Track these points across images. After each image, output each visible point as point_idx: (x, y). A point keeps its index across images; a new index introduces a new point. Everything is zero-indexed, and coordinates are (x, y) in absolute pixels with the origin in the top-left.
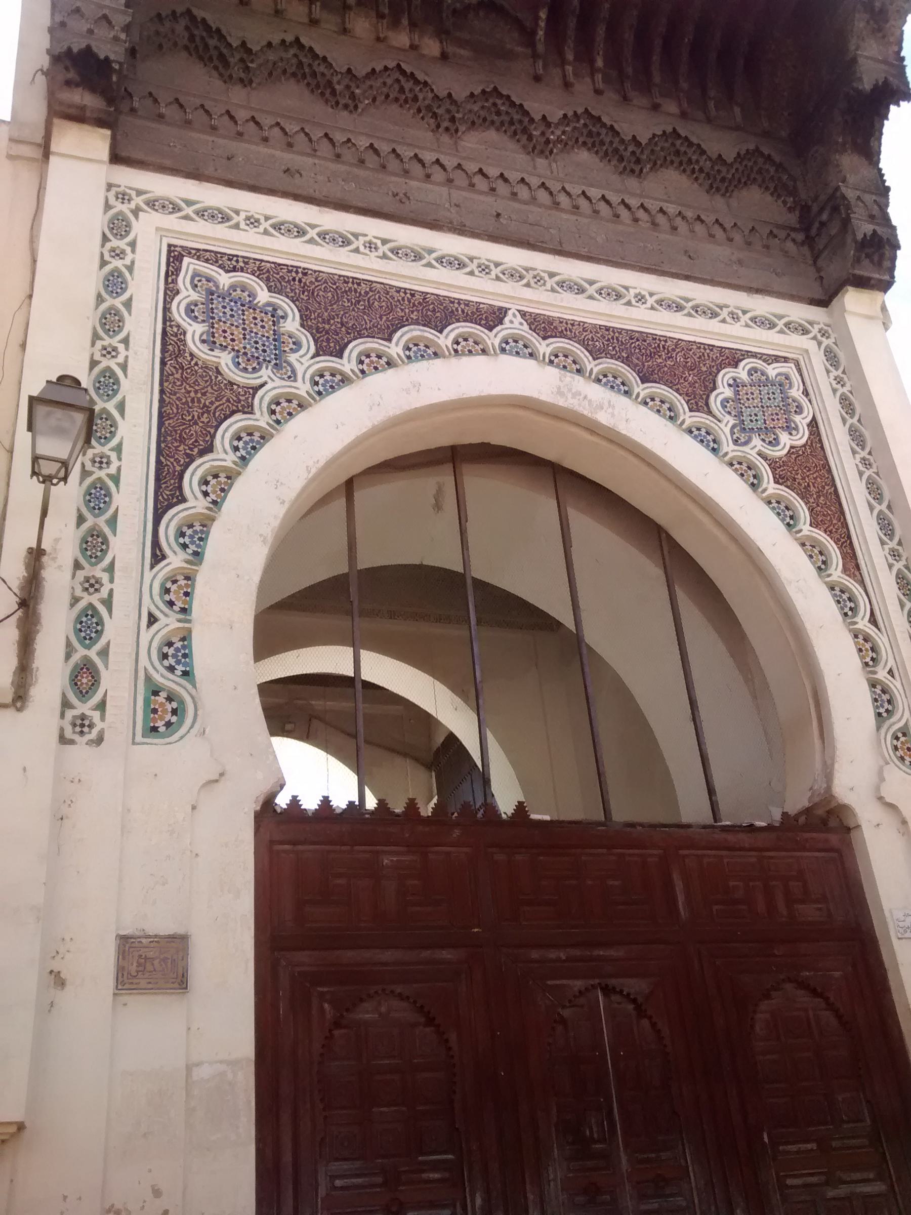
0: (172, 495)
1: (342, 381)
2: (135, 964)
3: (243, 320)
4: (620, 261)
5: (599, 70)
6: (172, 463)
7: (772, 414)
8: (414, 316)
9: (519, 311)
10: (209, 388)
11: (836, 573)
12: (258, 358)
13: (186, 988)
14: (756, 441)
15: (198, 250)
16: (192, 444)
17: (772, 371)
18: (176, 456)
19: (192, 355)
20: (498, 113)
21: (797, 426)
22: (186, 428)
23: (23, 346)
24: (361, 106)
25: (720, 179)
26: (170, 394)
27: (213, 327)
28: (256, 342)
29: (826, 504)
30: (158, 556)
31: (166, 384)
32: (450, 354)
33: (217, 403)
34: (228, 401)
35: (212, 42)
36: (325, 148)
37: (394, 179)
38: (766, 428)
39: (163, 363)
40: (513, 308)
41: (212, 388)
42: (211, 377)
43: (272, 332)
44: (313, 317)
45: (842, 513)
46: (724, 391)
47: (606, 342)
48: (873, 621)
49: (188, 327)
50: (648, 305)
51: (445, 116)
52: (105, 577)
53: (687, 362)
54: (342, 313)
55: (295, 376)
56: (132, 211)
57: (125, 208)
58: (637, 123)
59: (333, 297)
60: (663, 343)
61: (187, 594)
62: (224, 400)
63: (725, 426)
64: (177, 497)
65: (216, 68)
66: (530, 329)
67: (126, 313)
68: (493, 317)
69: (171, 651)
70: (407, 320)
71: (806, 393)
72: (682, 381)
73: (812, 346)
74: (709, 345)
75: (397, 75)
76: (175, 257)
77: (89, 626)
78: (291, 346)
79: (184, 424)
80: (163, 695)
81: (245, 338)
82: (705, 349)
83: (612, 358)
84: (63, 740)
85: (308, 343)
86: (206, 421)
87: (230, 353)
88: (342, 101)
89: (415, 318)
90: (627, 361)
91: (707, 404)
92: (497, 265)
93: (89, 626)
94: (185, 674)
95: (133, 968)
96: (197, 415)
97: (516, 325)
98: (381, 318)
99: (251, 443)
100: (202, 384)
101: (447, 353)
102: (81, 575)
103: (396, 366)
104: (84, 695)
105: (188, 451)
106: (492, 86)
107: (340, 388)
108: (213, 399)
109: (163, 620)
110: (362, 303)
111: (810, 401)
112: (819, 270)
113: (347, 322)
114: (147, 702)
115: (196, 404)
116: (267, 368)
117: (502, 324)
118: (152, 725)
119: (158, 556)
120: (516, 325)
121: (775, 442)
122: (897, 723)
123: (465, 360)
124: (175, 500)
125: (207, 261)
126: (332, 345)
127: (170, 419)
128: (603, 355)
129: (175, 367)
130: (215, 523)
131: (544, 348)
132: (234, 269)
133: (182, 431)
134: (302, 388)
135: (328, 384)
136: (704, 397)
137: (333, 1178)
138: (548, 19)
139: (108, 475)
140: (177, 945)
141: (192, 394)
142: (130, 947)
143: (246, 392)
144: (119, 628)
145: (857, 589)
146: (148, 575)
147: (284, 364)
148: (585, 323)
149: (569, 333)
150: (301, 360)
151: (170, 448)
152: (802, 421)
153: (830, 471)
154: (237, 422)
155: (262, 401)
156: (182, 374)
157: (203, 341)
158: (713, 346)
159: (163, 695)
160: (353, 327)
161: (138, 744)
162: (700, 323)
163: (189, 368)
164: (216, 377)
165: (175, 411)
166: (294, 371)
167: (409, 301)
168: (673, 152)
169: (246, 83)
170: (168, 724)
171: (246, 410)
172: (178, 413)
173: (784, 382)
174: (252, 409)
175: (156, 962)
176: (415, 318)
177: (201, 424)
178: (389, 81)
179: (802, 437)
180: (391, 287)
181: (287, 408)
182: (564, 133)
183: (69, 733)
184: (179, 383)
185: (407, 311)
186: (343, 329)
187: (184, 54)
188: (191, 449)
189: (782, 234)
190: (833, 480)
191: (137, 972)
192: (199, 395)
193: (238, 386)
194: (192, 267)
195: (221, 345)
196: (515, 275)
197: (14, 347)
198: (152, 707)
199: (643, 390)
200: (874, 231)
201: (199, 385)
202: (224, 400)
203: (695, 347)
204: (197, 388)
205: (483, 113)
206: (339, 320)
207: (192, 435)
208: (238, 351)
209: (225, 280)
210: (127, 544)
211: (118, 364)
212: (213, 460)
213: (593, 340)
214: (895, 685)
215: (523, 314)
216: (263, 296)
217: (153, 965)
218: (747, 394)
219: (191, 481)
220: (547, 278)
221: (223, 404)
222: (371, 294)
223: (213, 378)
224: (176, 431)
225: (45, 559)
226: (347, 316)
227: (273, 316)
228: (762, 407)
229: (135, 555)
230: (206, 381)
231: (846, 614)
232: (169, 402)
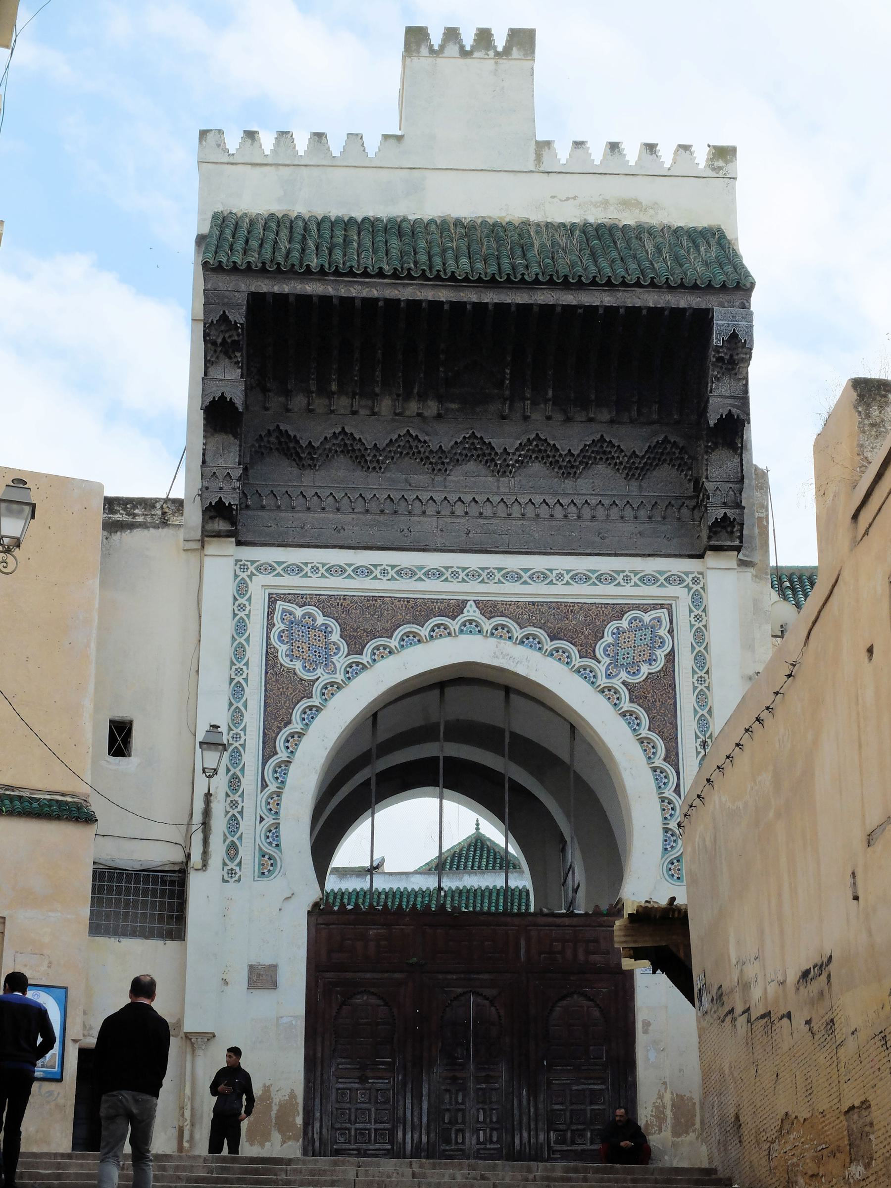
1: (362, 669)
4: (549, 551)
5: (549, 400)
11: (659, 762)
15: (285, 594)
17: (647, 618)
19: (281, 665)
20: (476, 449)
23: (198, 671)
24: (383, 466)
25: (635, 469)
30: (264, 785)
35: (291, 445)
36: (359, 506)
37: (402, 518)
39: (266, 673)
51: (439, 462)
52: (240, 800)
56: (248, 576)
57: (244, 575)
58: (572, 438)
61: (278, 804)
65: (294, 460)
67: (247, 646)
69: (270, 835)
75: (408, 438)
76: (272, 600)
77: (234, 824)
78: (335, 651)
80: (267, 857)
84: (224, 881)
85: (344, 648)
88: (371, 466)
92: (464, 569)
93: (234, 824)
94: (277, 845)
95: (255, 979)
96: (286, 699)
99: (314, 711)
102: (229, 799)
104: (232, 859)
106: (471, 432)
107: (361, 673)
109: (267, 819)
114: (260, 861)
119: (264, 785)
120: (471, 613)
123: (437, 641)
125: (289, 602)
132: (305, 605)
135: (355, 670)
137: (338, 1064)
138: (511, 373)
140: (273, 969)
144: (247, 825)
145: (670, 771)
146: (260, 796)
152: (661, 654)
157: (287, 655)
159: (267, 857)
160: (371, 632)
168: (599, 452)
169: (312, 467)
170: (269, 871)
178: (402, 444)
182: (520, 456)
183: (226, 878)
187: (276, 454)
194: (281, 607)
196: (474, 575)
197: (194, 673)
200: (725, 513)
205: (464, 452)
209: (299, 612)
210: (249, 782)
216: (320, 620)
217: (262, 978)
219: (280, 743)
225: (212, 798)
226: (367, 623)
229: (253, 787)
231: (660, 787)
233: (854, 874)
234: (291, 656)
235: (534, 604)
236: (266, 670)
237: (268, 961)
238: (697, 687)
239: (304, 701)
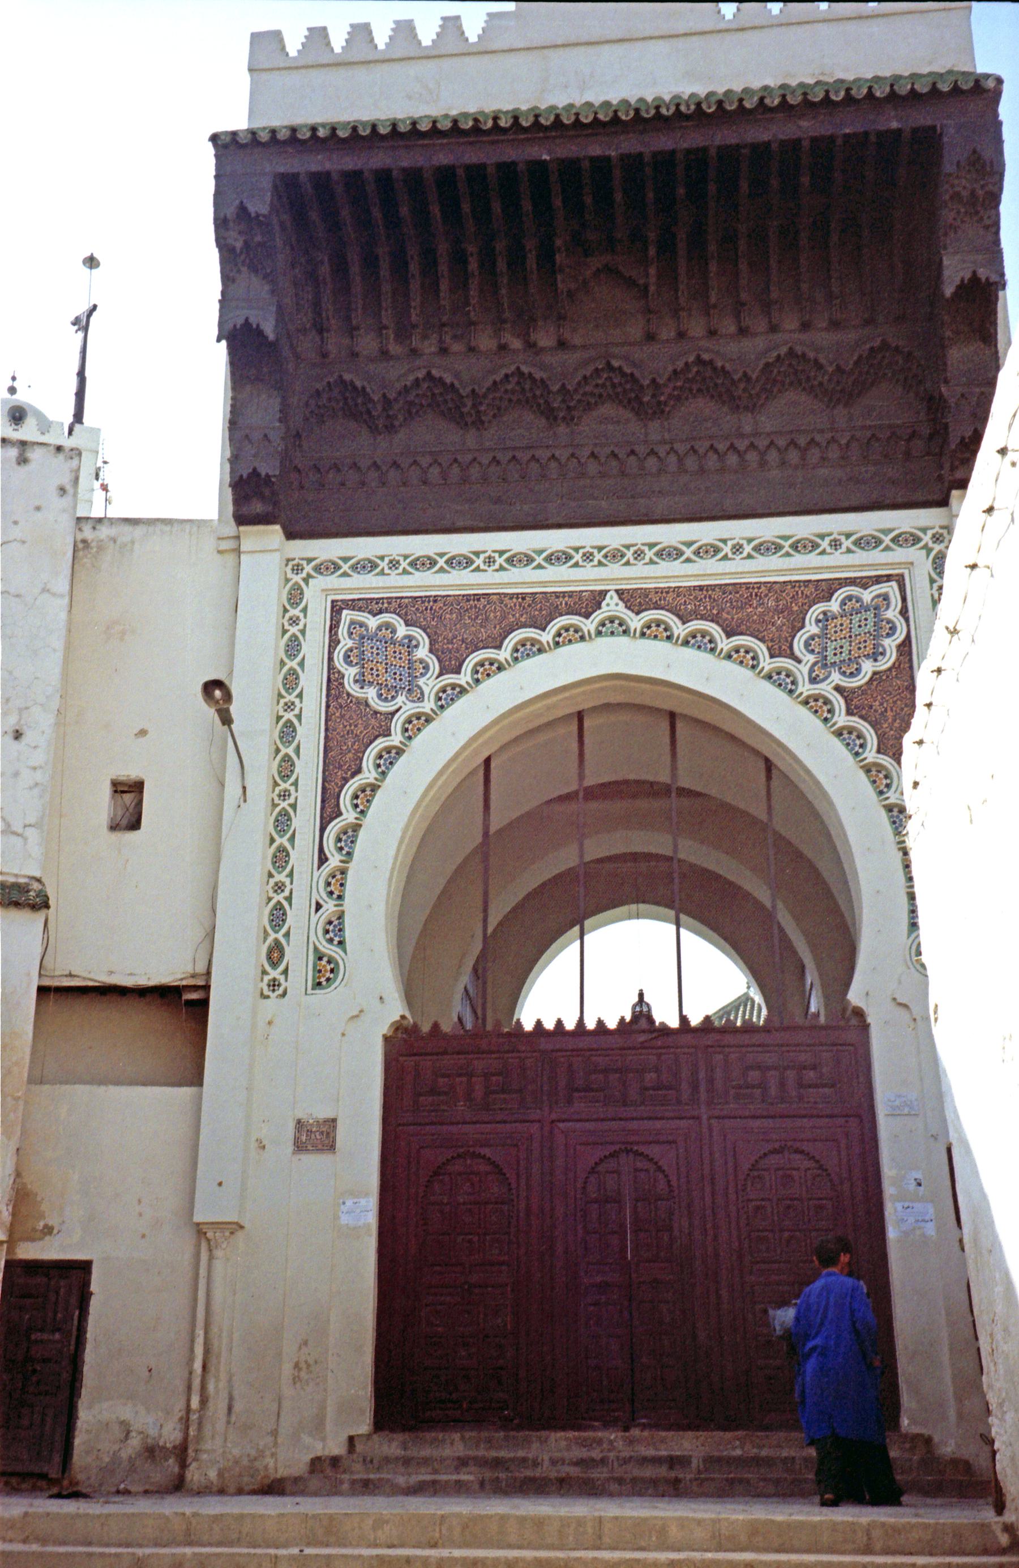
30: (323, 859)
119: (323, 859)
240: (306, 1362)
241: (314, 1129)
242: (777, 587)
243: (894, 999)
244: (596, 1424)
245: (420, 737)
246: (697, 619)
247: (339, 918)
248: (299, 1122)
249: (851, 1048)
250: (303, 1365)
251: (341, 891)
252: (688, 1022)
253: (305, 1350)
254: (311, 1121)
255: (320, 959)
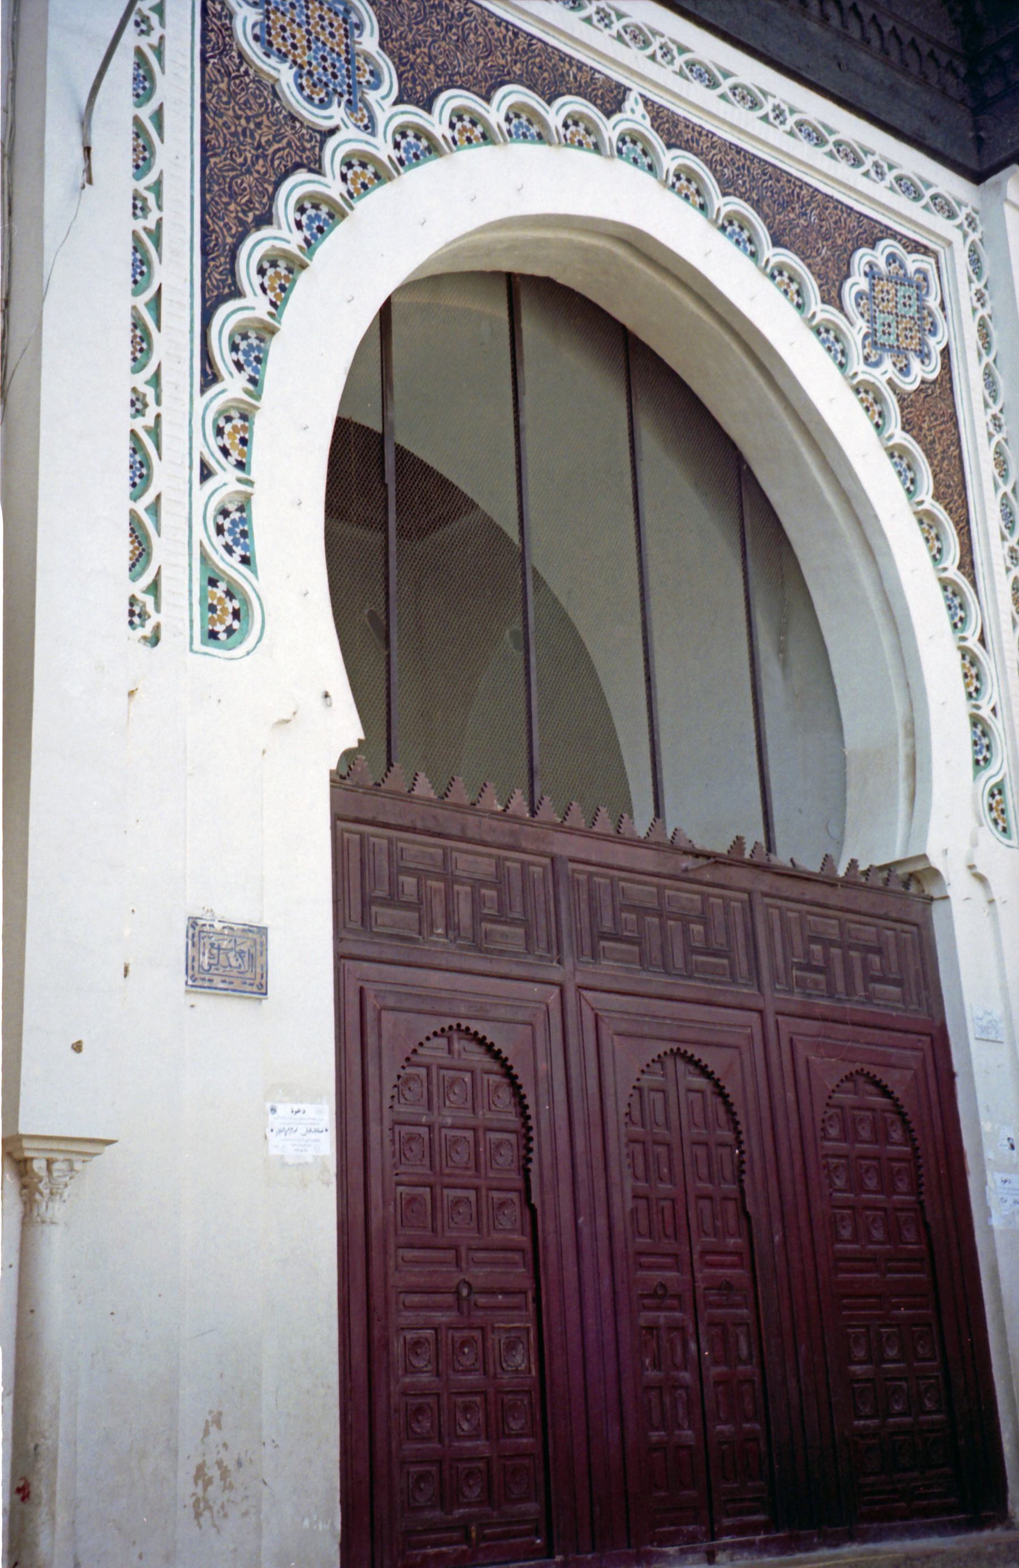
0: (224, 281)
2: (207, 955)
3: (307, 16)
6: (221, 229)
7: (906, 329)
8: (517, 69)
9: (641, 96)
10: (265, 117)
12: (326, 85)
13: (266, 994)
14: (887, 364)
16: (246, 204)
17: (913, 262)
18: (226, 220)
19: (241, 55)
21: (929, 352)
22: (237, 176)
26: (215, 113)
27: (269, 18)
28: (324, 58)
29: (949, 470)
30: (210, 377)
31: (209, 96)
32: (560, 143)
33: (276, 146)
34: (289, 144)
38: (898, 347)
40: (636, 89)
41: (268, 118)
42: (266, 99)
43: (343, 47)
44: (394, 36)
45: (965, 488)
46: (857, 282)
47: (743, 173)
48: (982, 640)
49: (237, 8)
50: (787, 127)
53: (821, 227)
54: (430, 39)
55: (374, 126)
59: (419, 11)
60: (797, 190)
62: (285, 141)
63: (856, 332)
64: (229, 286)
66: (652, 126)
68: (611, 98)
70: (509, 73)
71: (943, 306)
72: (814, 254)
73: (956, 236)
74: (847, 207)
79: (234, 169)
81: (309, 48)
82: (842, 211)
83: (741, 197)
86: (263, 170)
87: (291, 68)
89: (518, 72)
90: (756, 205)
91: (839, 296)
97: (637, 117)
98: (477, 60)
99: (321, 218)
100: (255, 107)
101: (557, 140)
103: (494, 143)
105: (241, 215)
108: (270, 137)
110: (454, 30)
111: (945, 317)
112: (977, 128)
113: (436, 57)
115: (249, 140)
116: (339, 104)
117: (620, 111)
118: (210, 627)
119: (210, 377)
121: (905, 371)
122: (992, 774)
124: (227, 290)
126: (419, 88)
127: (215, 155)
128: (731, 190)
129: (219, 71)
130: (275, 338)
131: (671, 160)
133: (232, 178)
134: (383, 149)
135: (419, 147)
136: (837, 284)
139: (145, 229)
140: (201, 978)
141: (243, 122)
142: (200, 932)
143: (311, 137)
147: (360, 105)
148: (714, 134)
149: (695, 145)
150: (382, 102)
151: (217, 203)
153: (956, 425)
154: (297, 185)
155: (334, 153)
156: (229, 85)
158: (851, 209)
161: (196, 652)
162: (842, 170)
163: (237, 77)
164: (273, 103)
165: (222, 144)
166: (372, 118)
167: (512, 42)
171: (312, 166)
172: (225, 148)
173: (920, 284)
174: (320, 167)
175: (231, 954)
176: (518, 72)
177: (256, 175)
179: (932, 371)
180: (492, 14)
181: (367, 173)
184: (225, 99)
185: (509, 58)
186: (432, 67)
188: (245, 212)
189: (944, 59)
190: (959, 440)
191: (210, 965)
192: (252, 126)
193: (302, 124)
195: (279, 50)
198: (210, 601)
199: (774, 255)
201: (251, 109)
202: (285, 141)
203: (831, 205)
204: (250, 113)
206: (426, 50)
207: (245, 189)
208: (301, 67)
211: (151, 46)
212: (275, 238)
213: (721, 164)
214: (997, 725)
215: (646, 101)
218: (882, 292)
220: (675, 52)
221: (283, 149)
222: (466, 19)
223: (269, 101)
224: (224, 178)
227: (345, 21)
228: (897, 314)
230: (261, 105)
232: (214, 128)
233: (225, 484)
234: (263, 38)
235: (739, 150)
236: (203, 52)
237: (207, 1004)
238: (146, 591)
239: (301, 175)
240: (219, 1464)
241: (224, 944)
242: (819, 197)
243: (971, 867)
244: (671, 1550)
245: (820, 349)
246: (735, 195)
247: (241, 509)
248: (193, 923)
249: (914, 929)
250: (214, 1472)
251: (242, 453)
252: (857, 867)
253: (215, 1436)
254: (218, 926)
255: (213, 582)
